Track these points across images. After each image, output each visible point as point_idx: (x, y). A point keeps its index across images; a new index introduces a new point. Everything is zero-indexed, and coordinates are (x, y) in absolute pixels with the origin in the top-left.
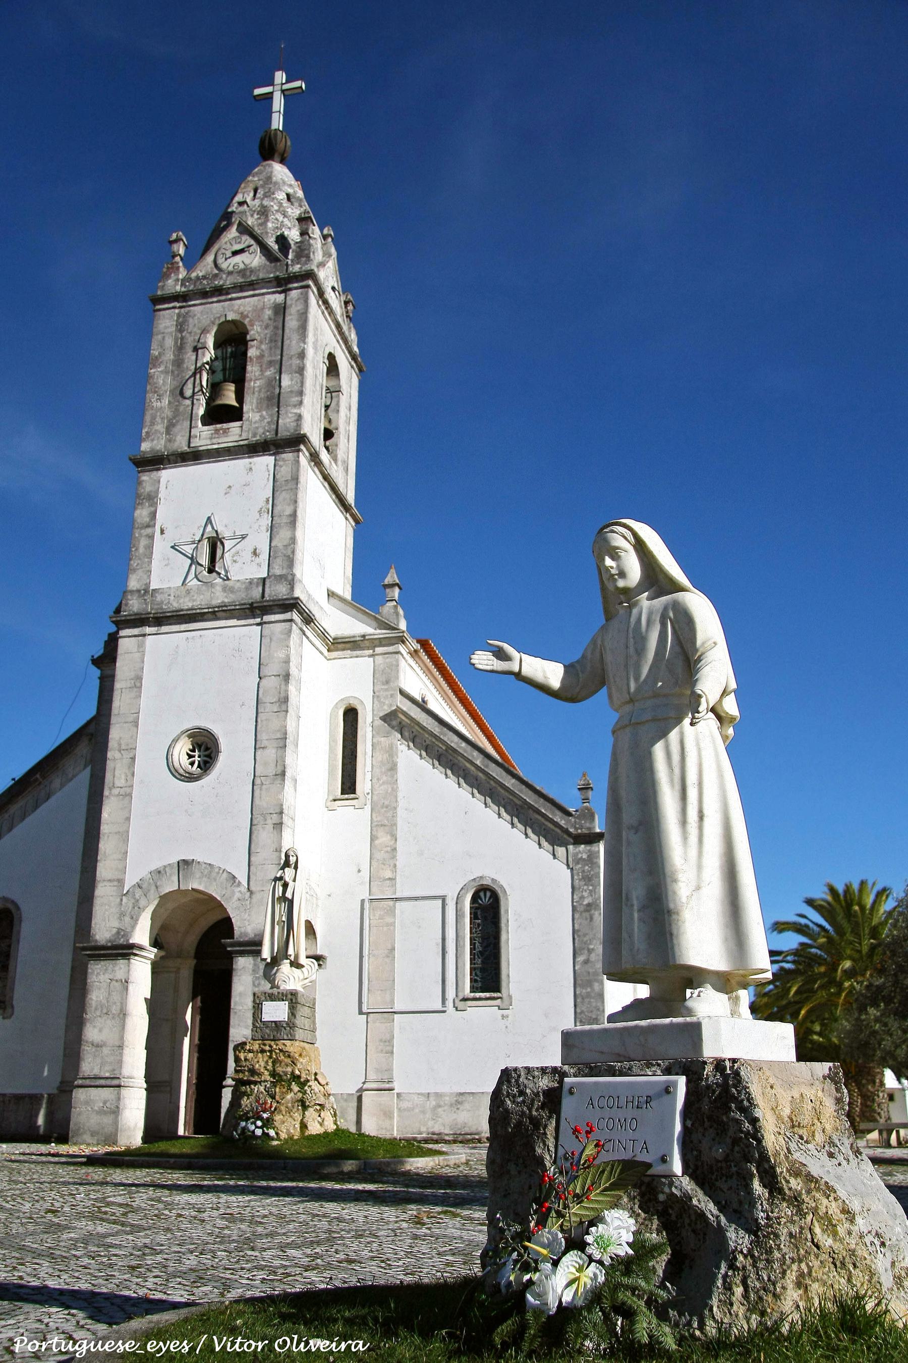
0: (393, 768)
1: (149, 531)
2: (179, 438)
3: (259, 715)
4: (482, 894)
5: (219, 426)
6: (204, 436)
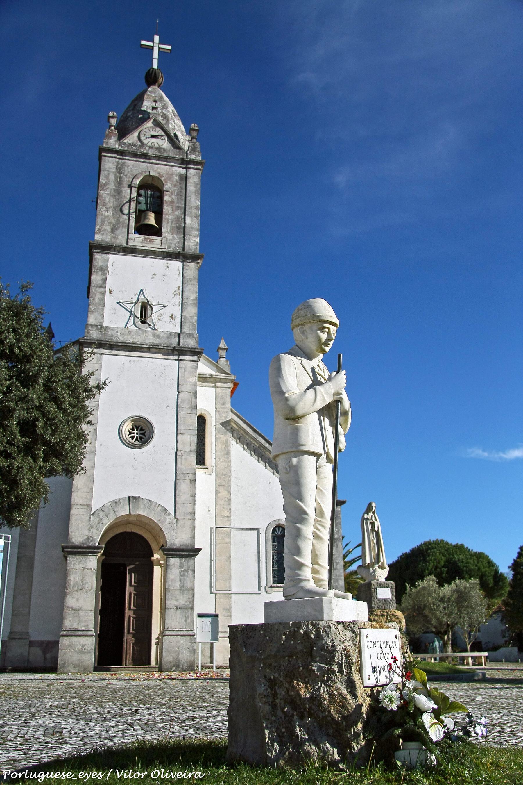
0: (228, 453)
1: (102, 290)
2: (120, 237)
3: (179, 414)
4: (277, 529)
5: (146, 236)
6: (137, 240)
